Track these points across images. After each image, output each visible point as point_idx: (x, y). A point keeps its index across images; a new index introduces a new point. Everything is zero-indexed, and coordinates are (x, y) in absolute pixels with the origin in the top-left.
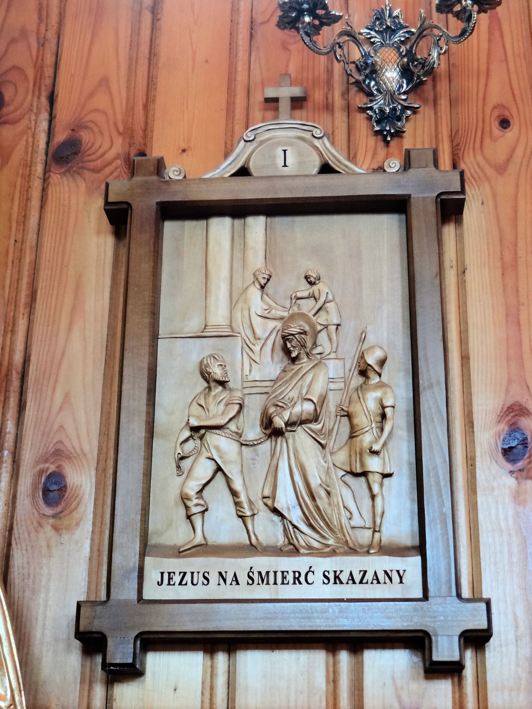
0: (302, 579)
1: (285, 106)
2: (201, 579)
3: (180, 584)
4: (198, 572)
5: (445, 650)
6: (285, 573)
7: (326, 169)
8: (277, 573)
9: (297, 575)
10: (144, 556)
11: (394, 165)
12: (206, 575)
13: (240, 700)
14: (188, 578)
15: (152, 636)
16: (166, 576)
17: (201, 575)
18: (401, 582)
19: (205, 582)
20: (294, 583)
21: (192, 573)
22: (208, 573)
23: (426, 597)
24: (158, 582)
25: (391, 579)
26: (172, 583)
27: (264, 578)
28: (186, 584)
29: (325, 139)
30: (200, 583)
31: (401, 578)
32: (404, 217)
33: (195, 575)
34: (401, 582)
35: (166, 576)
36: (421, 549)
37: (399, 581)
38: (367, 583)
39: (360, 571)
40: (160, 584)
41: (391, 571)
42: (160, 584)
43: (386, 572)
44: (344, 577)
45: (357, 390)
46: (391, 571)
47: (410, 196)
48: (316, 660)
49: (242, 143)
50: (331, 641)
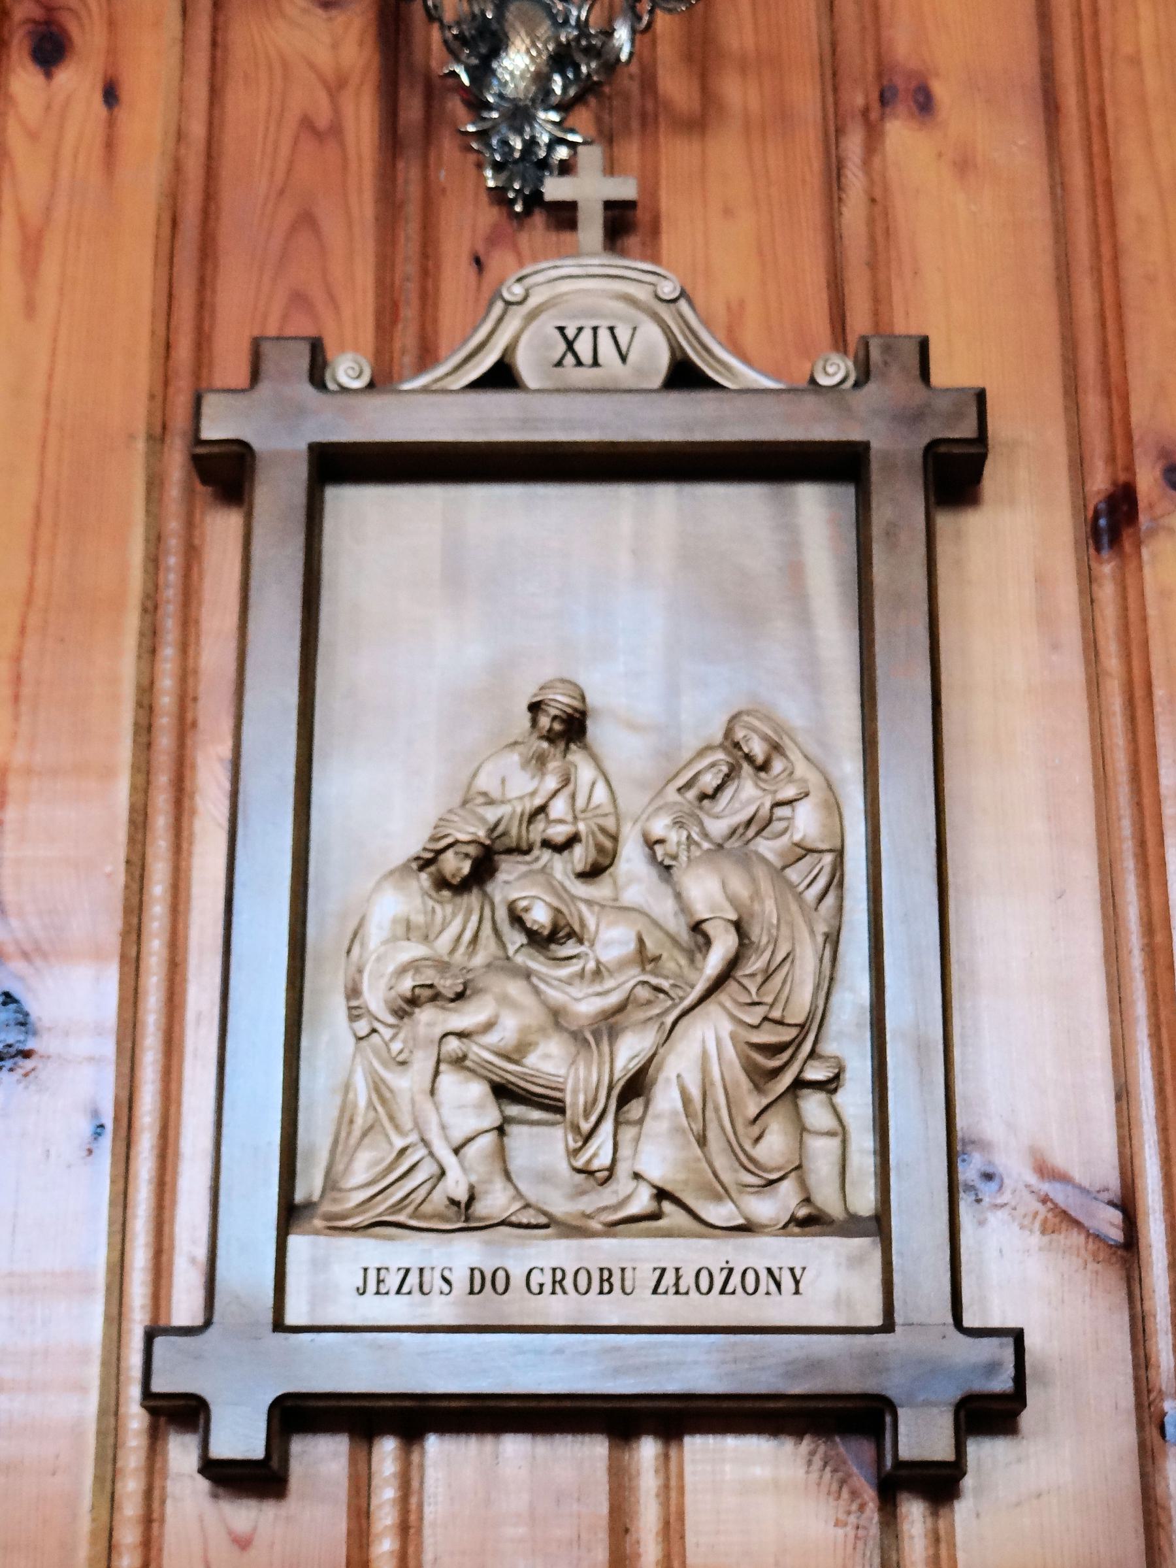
0: (568, 1283)
1: (591, 229)
2: (439, 1284)
3: (398, 1292)
4: (433, 1269)
5: (923, 1436)
6: (383, 1272)
7: (684, 376)
8: (369, 1272)
9: (606, 1275)
10: (287, 1234)
11: (830, 370)
12: (447, 1274)
13: (693, 1555)
14: (413, 1279)
15: (433, 1404)
16: (372, 1276)
17: (437, 1274)
18: (797, 1292)
19: (446, 1288)
20: (553, 1293)
21: (421, 1270)
22: (450, 1269)
23: (888, 1326)
24: (358, 1289)
25: (778, 1285)
26: (383, 1290)
27: (606, 1281)
28: (733, 1293)
29: (683, 305)
30: (762, 1289)
31: (797, 1282)
32: (847, 493)
33: (427, 1273)
34: (797, 1292)
35: (372, 1276)
36: (879, 1225)
37: (468, 1290)
38: (666, 1293)
39: (655, 1269)
40: (362, 1292)
41: (781, 1269)
42: (362, 1292)
43: (769, 1271)
44: (518, 1280)
45: (615, 838)
46: (781, 1269)
47: (865, 446)
48: (594, 1450)
49: (499, 306)
50: (618, 1419)
